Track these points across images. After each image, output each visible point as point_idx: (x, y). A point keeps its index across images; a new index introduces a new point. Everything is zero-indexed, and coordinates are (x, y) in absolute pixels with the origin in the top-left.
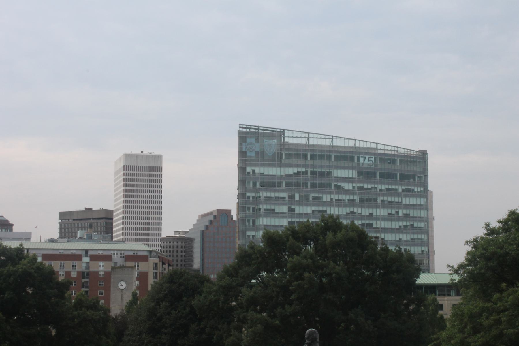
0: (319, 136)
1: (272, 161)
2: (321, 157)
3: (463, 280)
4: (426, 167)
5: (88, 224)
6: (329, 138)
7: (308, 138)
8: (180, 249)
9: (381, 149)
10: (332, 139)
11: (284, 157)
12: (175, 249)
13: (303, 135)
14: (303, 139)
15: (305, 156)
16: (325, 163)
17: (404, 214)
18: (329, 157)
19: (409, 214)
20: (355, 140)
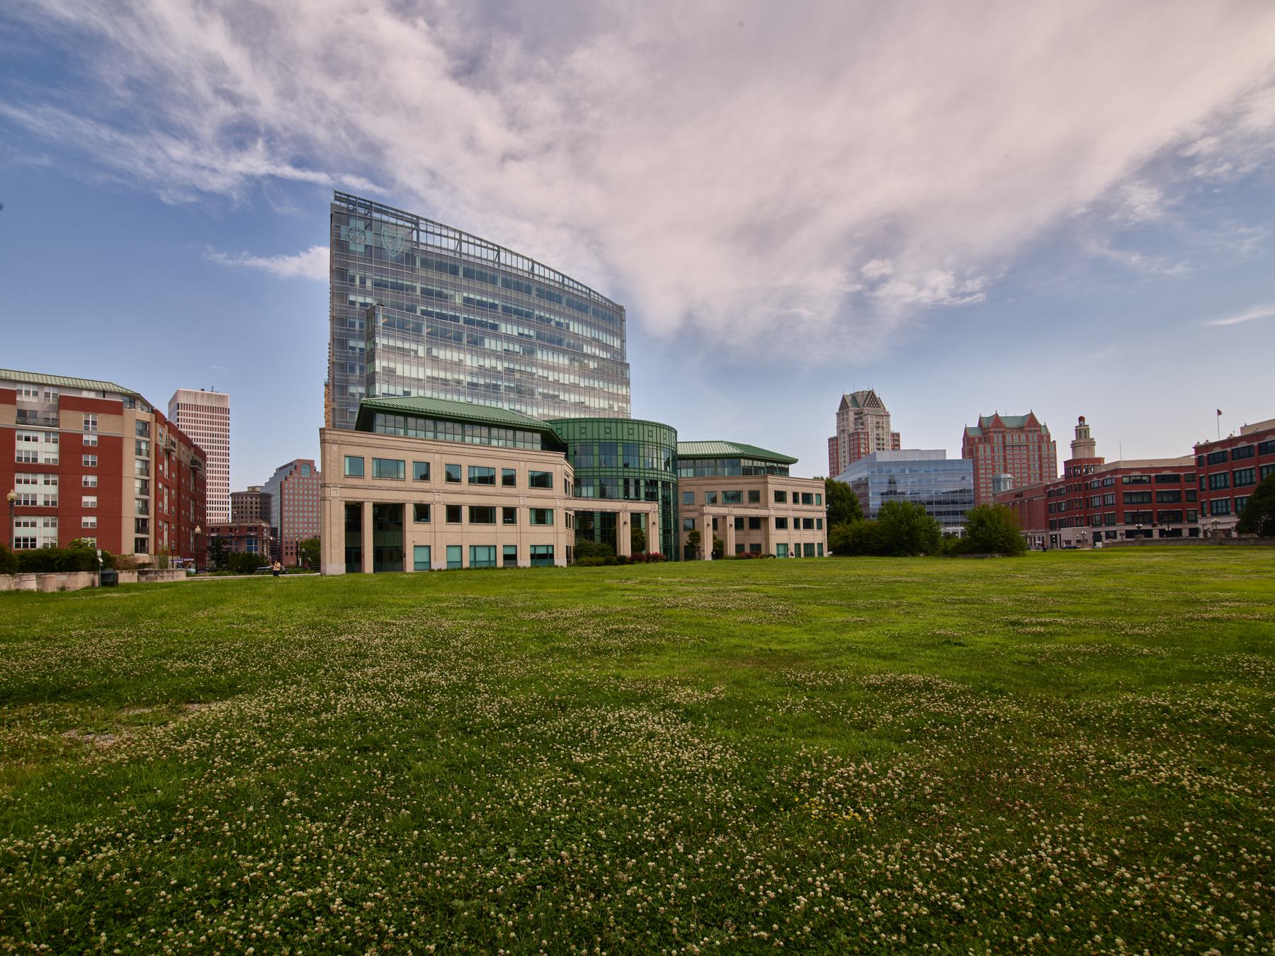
0: (478, 242)
1: (397, 266)
2: (441, 267)
3: (224, 565)
4: (1051, 451)
5: (1245, 501)
6: (493, 250)
7: (460, 241)
8: (254, 506)
9: (426, 245)
10: (499, 252)
11: (418, 264)
12: (249, 505)
13: (451, 234)
14: (452, 241)
15: (454, 271)
16: (446, 277)
17: (428, 377)
18: (528, 290)
19: (583, 403)
20: (533, 262)
